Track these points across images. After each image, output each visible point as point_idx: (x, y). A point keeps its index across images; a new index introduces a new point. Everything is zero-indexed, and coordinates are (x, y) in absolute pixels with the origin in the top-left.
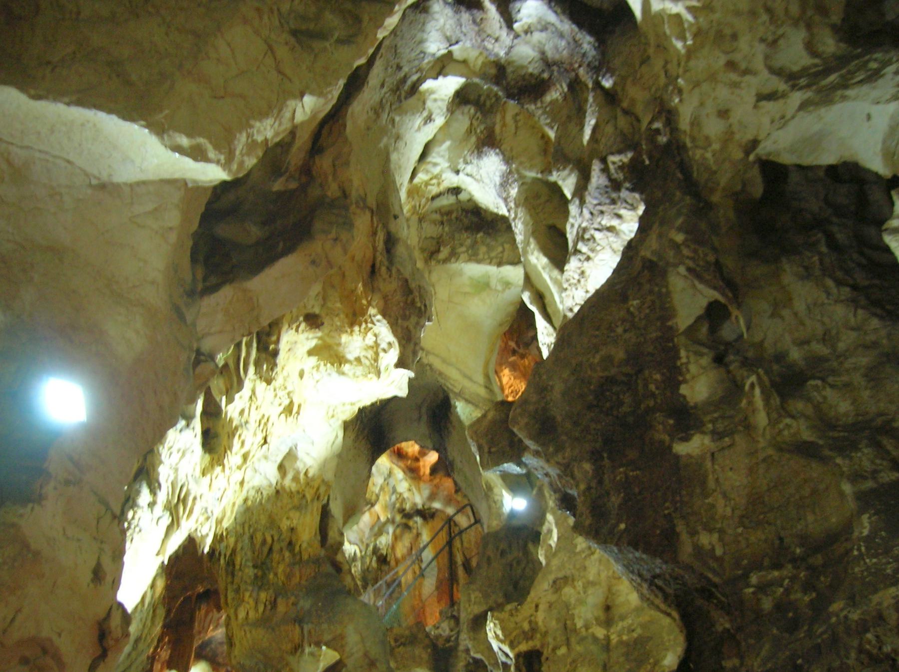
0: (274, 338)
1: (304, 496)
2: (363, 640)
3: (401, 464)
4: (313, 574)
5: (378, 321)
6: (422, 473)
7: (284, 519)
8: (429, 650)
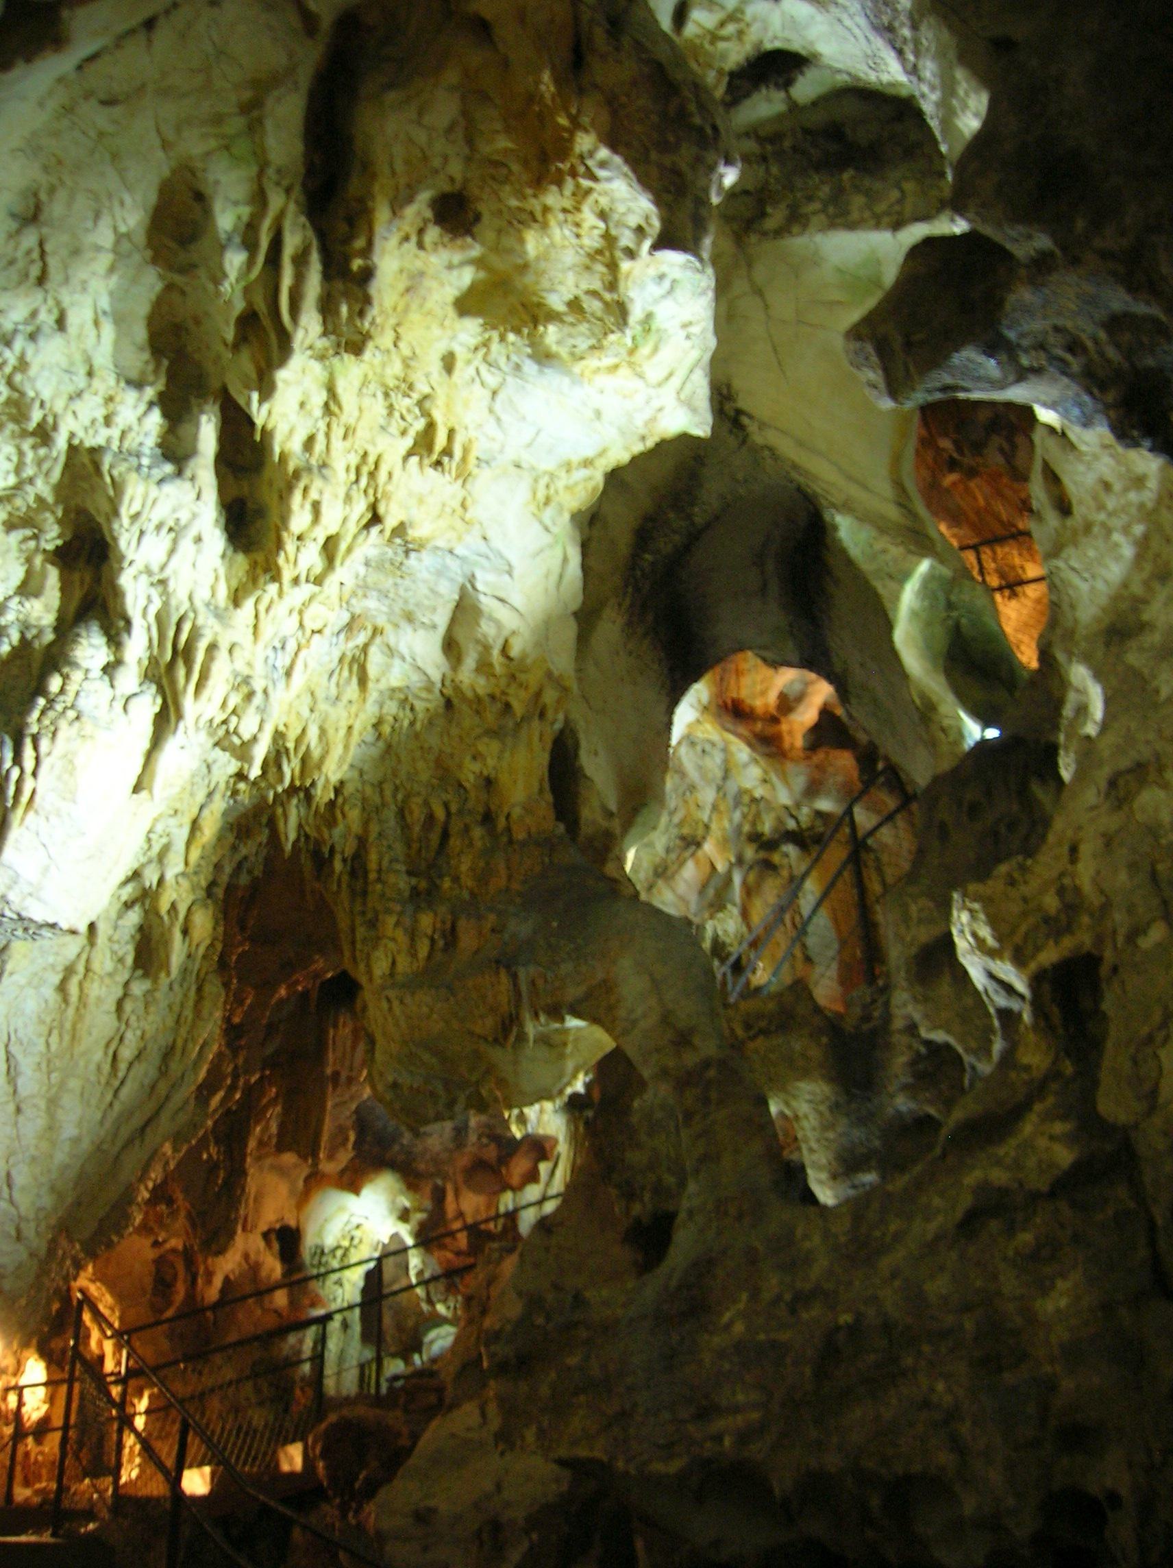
0: (360, 243)
1: (508, 706)
2: (656, 984)
3: (742, 730)
4: (538, 869)
5: (603, 164)
6: (786, 745)
7: (468, 759)
8: (824, 1040)
